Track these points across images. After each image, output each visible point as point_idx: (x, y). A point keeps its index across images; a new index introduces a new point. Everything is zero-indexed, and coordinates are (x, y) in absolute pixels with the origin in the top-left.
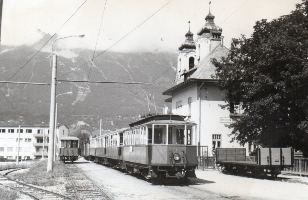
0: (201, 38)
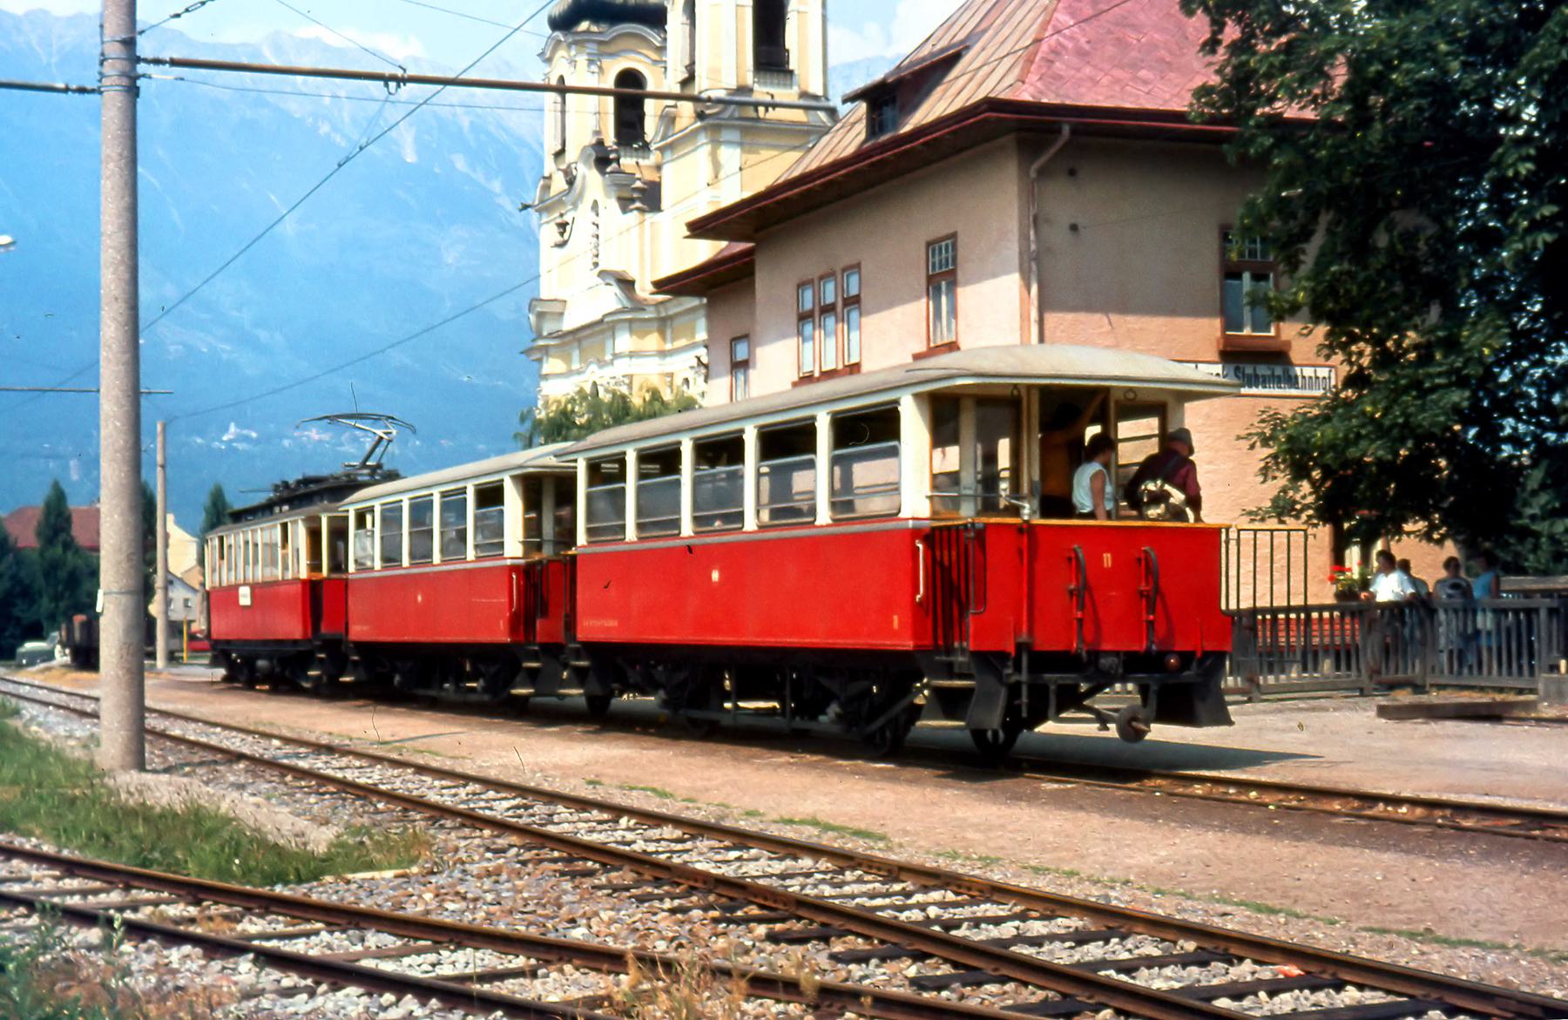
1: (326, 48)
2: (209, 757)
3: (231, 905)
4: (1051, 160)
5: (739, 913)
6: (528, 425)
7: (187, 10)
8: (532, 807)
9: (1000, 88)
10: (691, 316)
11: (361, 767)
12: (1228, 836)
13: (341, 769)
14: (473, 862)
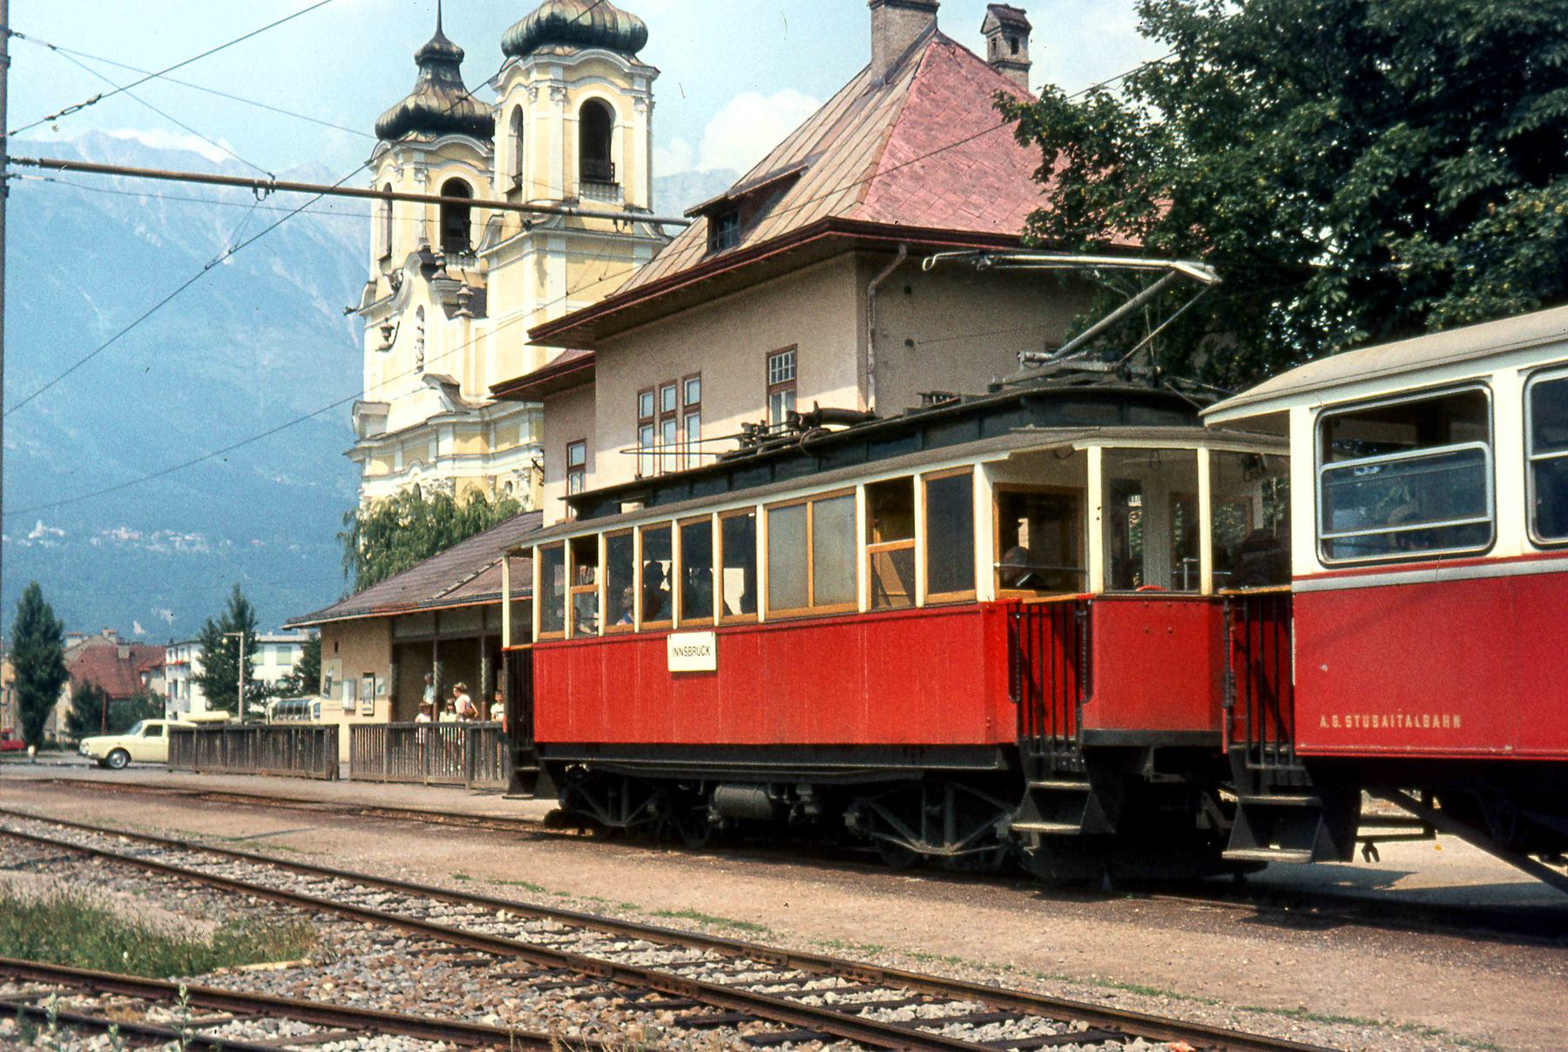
0: (528, 71)
1: (143, 148)
2: (60, 854)
3: (131, 997)
4: (890, 278)
5: (642, 1000)
6: (351, 526)
7: (63, 113)
8: (404, 901)
9: (838, 208)
10: (516, 420)
11: (218, 863)
12: (1095, 924)
13: (198, 865)
14: (362, 954)
